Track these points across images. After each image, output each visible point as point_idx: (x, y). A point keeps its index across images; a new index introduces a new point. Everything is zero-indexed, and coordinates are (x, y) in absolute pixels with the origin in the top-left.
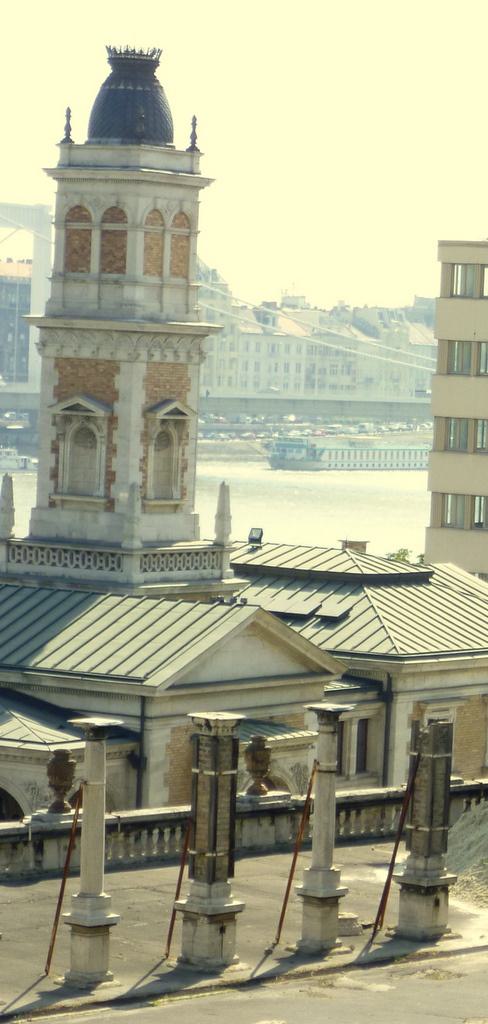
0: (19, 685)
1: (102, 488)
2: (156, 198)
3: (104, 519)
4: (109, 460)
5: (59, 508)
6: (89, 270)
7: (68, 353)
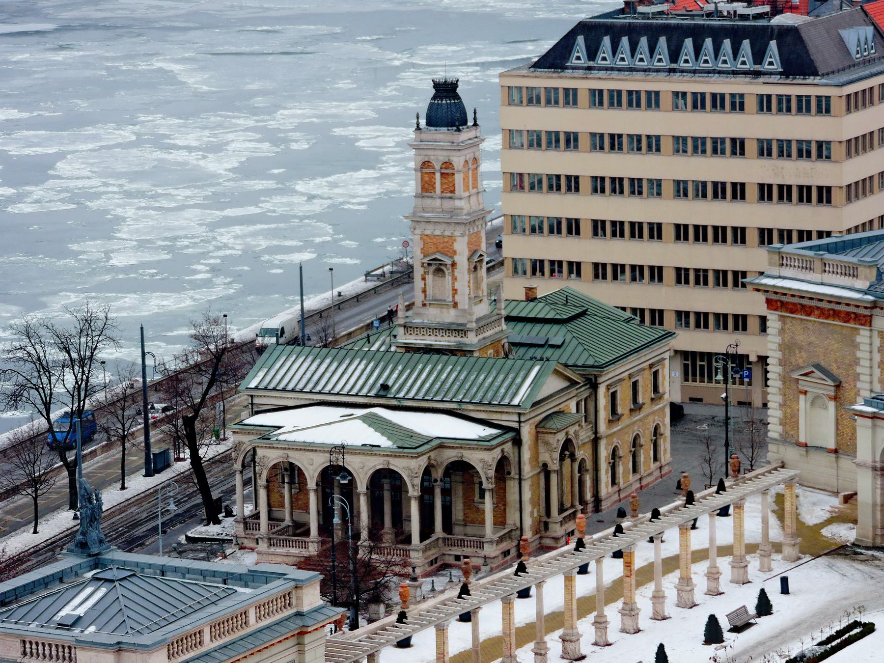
0: (457, 409)
1: (451, 297)
2: (466, 155)
3: (453, 312)
4: (453, 284)
5: (428, 307)
6: (435, 192)
7: (428, 232)
